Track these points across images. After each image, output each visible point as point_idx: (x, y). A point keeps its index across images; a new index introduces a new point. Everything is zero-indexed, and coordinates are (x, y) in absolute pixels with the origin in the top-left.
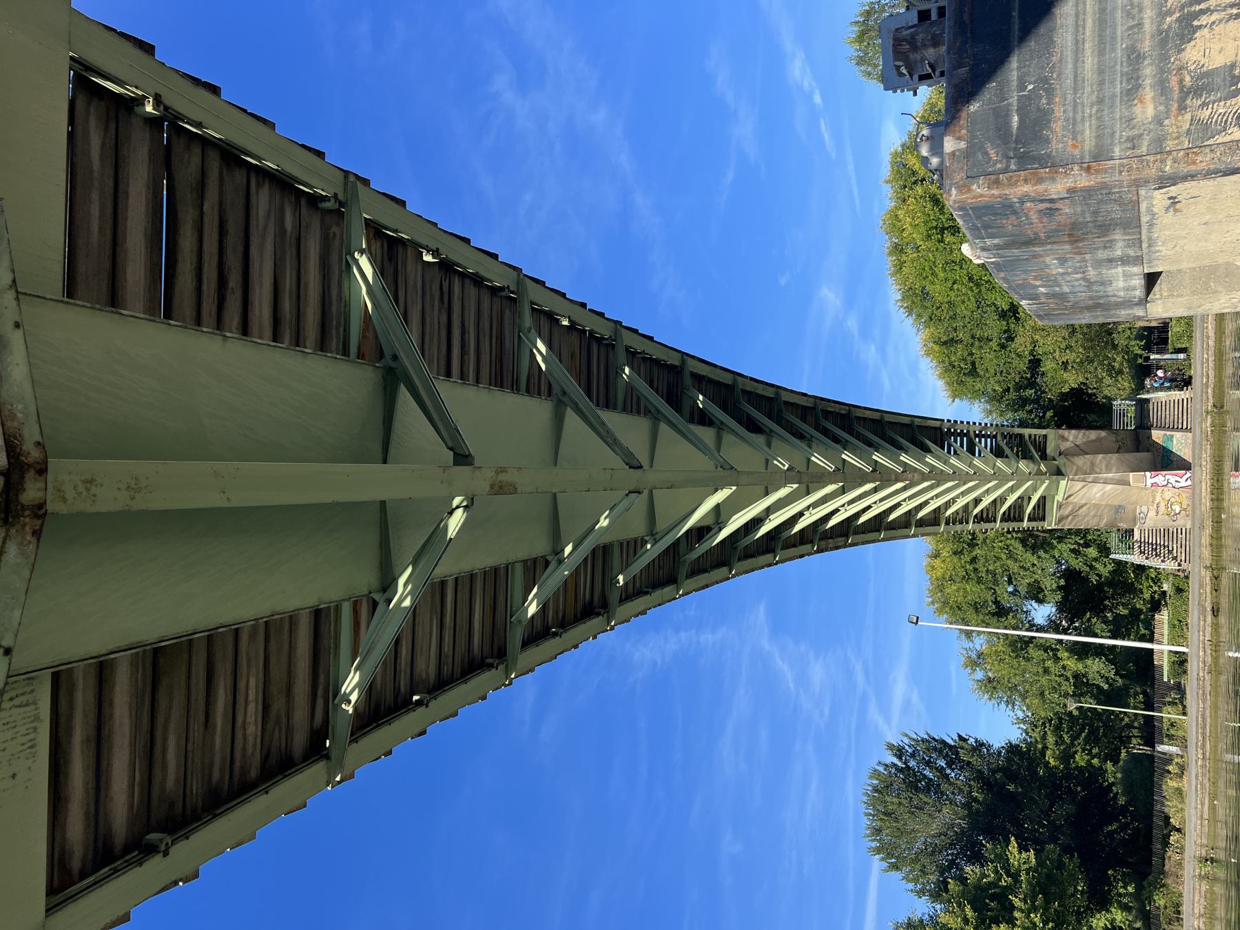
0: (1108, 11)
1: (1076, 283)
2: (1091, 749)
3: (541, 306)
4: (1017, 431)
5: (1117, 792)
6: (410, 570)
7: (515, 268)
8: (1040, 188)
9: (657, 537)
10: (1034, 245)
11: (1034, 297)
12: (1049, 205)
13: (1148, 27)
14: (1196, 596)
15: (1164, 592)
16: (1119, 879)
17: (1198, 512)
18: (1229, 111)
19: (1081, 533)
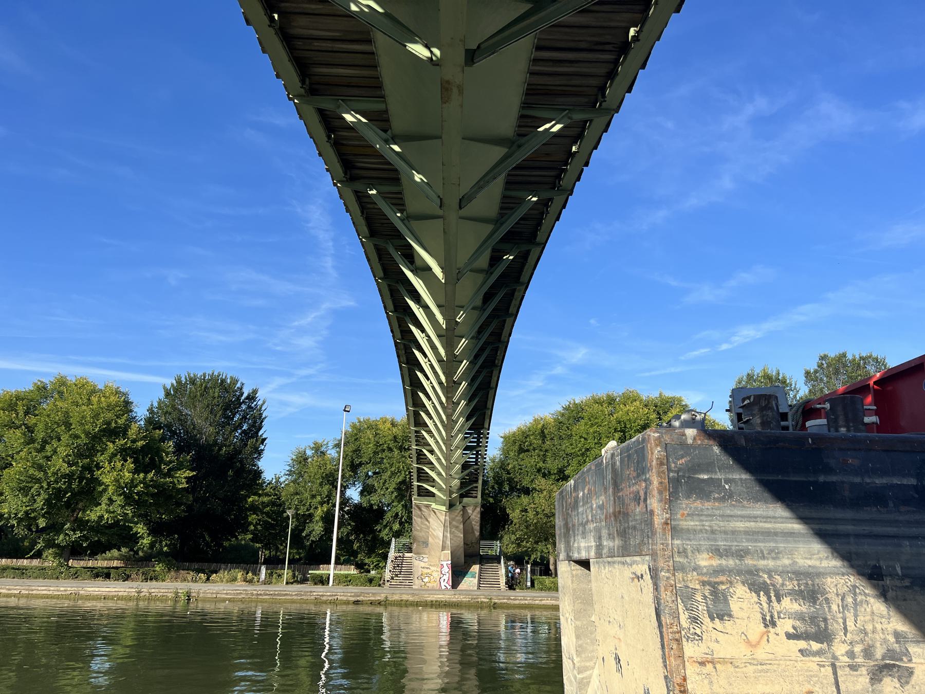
0: (775, 538)
1: (584, 516)
2: (261, 525)
3: (588, 129)
4: (481, 478)
5: (231, 541)
6: (380, 10)
7: (619, 107)
8: (655, 492)
9: (406, 221)
10: (614, 489)
11: (576, 488)
12: (642, 498)
13: (762, 563)
14: (366, 591)
15: (369, 571)
16: (171, 541)
17: (424, 592)
18: (700, 613)
19: (409, 519)
